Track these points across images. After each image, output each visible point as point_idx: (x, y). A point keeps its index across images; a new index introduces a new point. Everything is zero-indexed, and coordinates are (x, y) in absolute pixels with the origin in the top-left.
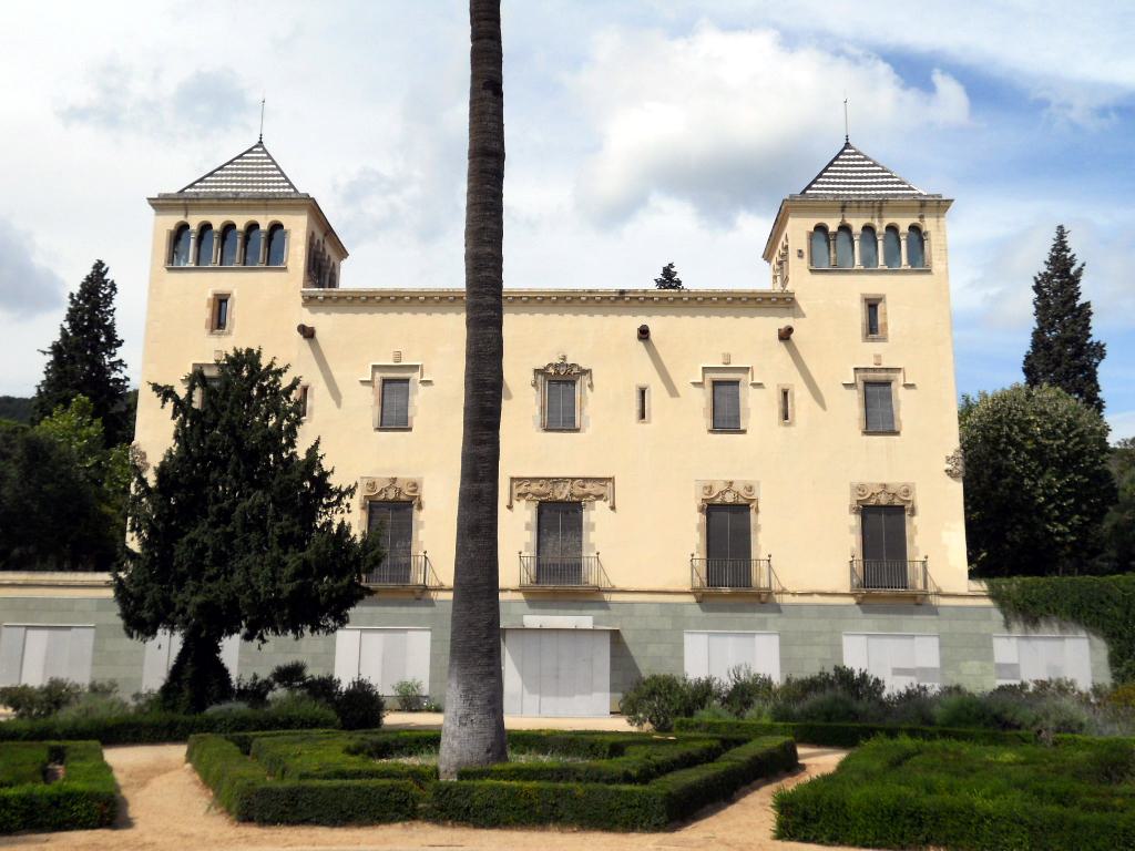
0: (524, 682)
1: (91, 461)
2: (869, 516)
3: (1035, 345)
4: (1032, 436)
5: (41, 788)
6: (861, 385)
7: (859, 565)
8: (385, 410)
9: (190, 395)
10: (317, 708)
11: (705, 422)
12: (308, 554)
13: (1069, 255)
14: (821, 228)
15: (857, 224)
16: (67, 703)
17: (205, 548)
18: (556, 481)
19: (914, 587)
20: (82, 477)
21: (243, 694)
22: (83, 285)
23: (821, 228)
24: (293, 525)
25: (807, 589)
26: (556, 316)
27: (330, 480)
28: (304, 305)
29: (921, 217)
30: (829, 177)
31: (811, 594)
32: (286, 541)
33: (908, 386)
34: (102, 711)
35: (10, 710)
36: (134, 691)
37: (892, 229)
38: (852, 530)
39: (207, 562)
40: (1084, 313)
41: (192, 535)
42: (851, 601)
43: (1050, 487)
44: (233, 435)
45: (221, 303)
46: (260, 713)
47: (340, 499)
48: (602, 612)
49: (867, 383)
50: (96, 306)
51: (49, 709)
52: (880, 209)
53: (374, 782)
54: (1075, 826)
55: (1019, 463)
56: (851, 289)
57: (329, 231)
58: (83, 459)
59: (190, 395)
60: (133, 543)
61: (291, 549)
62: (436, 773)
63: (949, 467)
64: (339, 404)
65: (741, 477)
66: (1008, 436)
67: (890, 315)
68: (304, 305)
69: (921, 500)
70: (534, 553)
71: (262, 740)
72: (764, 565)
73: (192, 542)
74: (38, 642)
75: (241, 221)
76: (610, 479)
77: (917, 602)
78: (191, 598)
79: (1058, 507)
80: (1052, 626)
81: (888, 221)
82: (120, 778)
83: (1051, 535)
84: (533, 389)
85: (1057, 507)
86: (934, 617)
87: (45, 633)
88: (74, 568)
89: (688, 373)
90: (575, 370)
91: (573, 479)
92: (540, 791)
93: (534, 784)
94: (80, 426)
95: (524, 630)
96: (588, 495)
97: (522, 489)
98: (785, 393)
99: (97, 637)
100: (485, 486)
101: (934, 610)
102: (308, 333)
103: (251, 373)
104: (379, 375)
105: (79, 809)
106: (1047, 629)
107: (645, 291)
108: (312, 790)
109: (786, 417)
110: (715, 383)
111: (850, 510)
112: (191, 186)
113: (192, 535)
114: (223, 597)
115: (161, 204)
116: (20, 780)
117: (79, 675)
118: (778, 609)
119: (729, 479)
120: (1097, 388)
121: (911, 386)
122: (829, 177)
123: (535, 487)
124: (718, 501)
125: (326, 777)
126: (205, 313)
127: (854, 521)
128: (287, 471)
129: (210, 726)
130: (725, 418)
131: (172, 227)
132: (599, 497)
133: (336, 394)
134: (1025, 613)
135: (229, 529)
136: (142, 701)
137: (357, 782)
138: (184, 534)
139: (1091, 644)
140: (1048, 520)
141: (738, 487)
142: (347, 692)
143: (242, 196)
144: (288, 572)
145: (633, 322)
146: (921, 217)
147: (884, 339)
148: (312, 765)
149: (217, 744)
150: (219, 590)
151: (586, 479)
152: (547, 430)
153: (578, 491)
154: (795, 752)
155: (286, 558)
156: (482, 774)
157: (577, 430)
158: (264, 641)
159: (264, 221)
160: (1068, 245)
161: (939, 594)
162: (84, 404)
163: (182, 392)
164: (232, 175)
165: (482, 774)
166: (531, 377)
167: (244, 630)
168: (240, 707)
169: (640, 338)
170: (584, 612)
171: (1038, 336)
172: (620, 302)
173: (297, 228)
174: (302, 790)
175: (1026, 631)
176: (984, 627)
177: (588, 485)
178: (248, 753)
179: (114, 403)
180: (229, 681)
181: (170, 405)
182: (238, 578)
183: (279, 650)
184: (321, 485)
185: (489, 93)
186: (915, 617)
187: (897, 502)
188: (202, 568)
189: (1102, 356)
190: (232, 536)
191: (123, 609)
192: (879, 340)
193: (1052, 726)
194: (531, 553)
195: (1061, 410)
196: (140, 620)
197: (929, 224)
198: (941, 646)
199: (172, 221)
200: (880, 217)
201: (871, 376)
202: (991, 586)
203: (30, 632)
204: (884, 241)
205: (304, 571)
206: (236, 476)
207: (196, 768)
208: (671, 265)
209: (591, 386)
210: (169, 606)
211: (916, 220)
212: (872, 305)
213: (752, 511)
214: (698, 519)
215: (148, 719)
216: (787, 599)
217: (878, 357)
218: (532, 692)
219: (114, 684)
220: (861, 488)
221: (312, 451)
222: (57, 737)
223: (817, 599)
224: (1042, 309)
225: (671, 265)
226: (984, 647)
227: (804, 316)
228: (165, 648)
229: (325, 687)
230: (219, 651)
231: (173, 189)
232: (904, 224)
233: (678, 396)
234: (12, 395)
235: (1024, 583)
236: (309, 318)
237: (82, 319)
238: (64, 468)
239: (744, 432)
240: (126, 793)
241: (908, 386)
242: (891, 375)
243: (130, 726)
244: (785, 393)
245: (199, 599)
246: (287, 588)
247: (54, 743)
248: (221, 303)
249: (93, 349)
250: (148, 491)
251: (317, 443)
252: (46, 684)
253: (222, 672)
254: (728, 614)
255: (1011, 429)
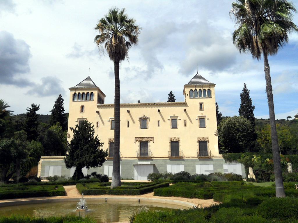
0: (138, 174)
1: (60, 134)
2: (200, 143)
3: (241, 107)
4: (236, 126)
5: (55, 190)
6: (199, 119)
7: (199, 152)
8: (112, 126)
9: (76, 129)
10: (97, 179)
11: (170, 126)
12: (95, 155)
13: (247, 89)
14: (191, 90)
15: (198, 89)
16: (57, 179)
17: (79, 154)
18: (143, 138)
19: (209, 156)
20: (58, 137)
21: (86, 177)
22: (57, 99)
23: (191, 90)
24: (93, 150)
25: (189, 156)
26: (143, 108)
27: (99, 142)
28: (97, 107)
29: (210, 88)
30: (196, 78)
31: (190, 157)
32: (92, 153)
33: (207, 119)
34: (63, 180)
35: (48, 180)
36: (68, 177)
37: (205, 90)
38: (197, 145)
39: (79, 156)
40: (250, 100)
41: (77, 152)
42: (197, 158)
43: (239, 135)
44: (83, 135)
45: (82, 107)
46: (88, 180)
47: (101, 145)
48: (152, 161)
49: (200, 119)
50: (60, 103)
51: (55, 180)
52: (202, 86)
53: (100, 189)
54: (187, 193)
55: (233, 131)
56: (197, 101)
57: (102, 93)
58: (59, 134)
59: (76, 129)
60: (67, 153)
61: (92, 154)
62: (110, 188)
63: (215, 134)
64: (104, 125)
65: (177, 137)
66: (231, 126)
67: (204, 106)
68: (97, 107)
69: (210, 140)
70: (139, 151)
71: (87, 184)
72: (181, 152)
73: (77, 153)
74: (52, 168)
75: (85, 92)
76: (153, 137)
77: (209, 158)
78: (77, 162)
79: (241, 139)
80: (234, 162)
81: (204, 88)
82: (66, 190)
83: (240, 144)
84: (139, 122)
85: (241, 139)
86: (212, 161)
87: (53, 167)
88: (58, 155)
89: (167, 118)
90: (146, 118)
91: (146, 137)
92: (123, 190)
93: (123, 189)
94: (58, 128)
95: (138, 165)
96: (149, 140)
97: (137, 140)
98: (185, 121)
99: (62, 167)
100: (117, 147)
101: (212, 160)
102: (98, 112)
103: (86, 125)
104: (111, 120)
105: (60, 193)
106: (233, 163)
107: (159, 103)
108: (92, 190)
109: (185, 125)
110: (172, 119)
111: (197, 141)
112: (76, 86)
113: (77, 152)
114: (82, 162)
115: (71, 89)
116: (52, 190)
117: (59, 174)
118: (184, 160)
119: (175, 137)
120: (253, 115)
121: (208, 119)
122: (196, 78)
123: (139, 139)
124: (173, 141)
125: (94, 189)
126: (80, 109)
127: (198, 144)
128: (92, 141)
129: (80, 182)
130: (174, 125)
131: (73, 94)
132: (151, 141)
133: (103, 123)
134: (229, 160)
135: (83, 151)
136: (69, 179)
137: (98, 189)
138: (75, 152)
139: (241, 165)
140: (239, 142)
141: (176, 138)
142: (103, 176)
143: (86, 87)
144: (92, 158)
145: (156, 109)
146: (210, 88)
147: (203, 111)
148: (92, 187)
149: (80, 185)
150: (81, 161)
151: (148, 137)
152: (141, 129)
153: (147, 140)
154: (169, 185)
155: (92, 156)
156: (117, 188)
157: (147, 129)
158: (89, 169)
159: (90, 92)
160: (247, 87)
161: (213, 157)
162: (58, 124)
163: (74, 128)
164: (84, 83)
165: (117, 188)
166: (138, 119)
167: (86, 167)
168: (85, 179)
169: (158, 112)
170: (46, 182)
171: (242, 105)
172: (154, 105)
173: (96, 93)
174: (90, 190)
175: (229, 163)
176: (222, 163)
177: (149, 139)
178: (85, 186)
179: (64, 122)
180: (83, 175)
181: (73, 131)
182: (84, 159)
183: (92, 170)
184: (98, 143)
185: (117, 87)
186: (209, 161)
187: (205, 140)
188: (78, 157)
189: (254, 109)
190: (83, 152)
191: (66, 164)
192: (202, 111)
193: (213, 180)
194: (139, 151)
195: (242, 121)
196: (69, 165)
197: (211, 89)
198: (214, 166)
199: (73, 92)
200: (202, 88)
201: (201, 117)
202: (223, 155)
203: (50, 167)
204: (203, 92)
205: (95, 157)
206: (83, 142)
207: (77, 189)
208: (171, 91)
209: (149, 121)
210: (73, 163)
211: (209, 88)
212: (201, 104)
213: (179, 143)
214: (169, 144)
215: (70, 181)
216: (186, 158)
217: (202, 114)
218: (139, 176)
219: (65, 176)
220: (199, 138)
221: (96, 137)
222: (56, 184)
223: (191, 158)
224: (242, 99)
225: (171, 91)
226: (222, 166)
227: (188, 106)
228: (73, 170)
229: (99, 176)
230: (81, 170)
231: (73, 87)
232: (207, 89)
233: (165, 122)
234: (43, 114)
235: (229, 155)
236: (98, 110)
237: (57, 106)
238: (55, 136)
239: (177, 128)
240: (66, 192)
241: (207, 119)
242: (205, 117)
243: (68, 182)
244: (185, 121)
245: (78, 162)
246: (92, 160)
247: (56, 185)
248: (82, 107)
249: (60, 112)
250: (69, 145)
251: (97, 136)
252: (54, 176)
253: (82, 174)
254: (175, 161)
255: (232, 125)
